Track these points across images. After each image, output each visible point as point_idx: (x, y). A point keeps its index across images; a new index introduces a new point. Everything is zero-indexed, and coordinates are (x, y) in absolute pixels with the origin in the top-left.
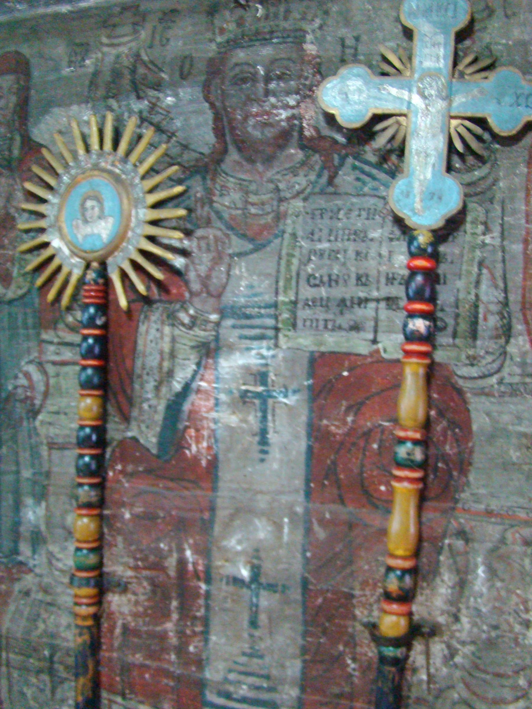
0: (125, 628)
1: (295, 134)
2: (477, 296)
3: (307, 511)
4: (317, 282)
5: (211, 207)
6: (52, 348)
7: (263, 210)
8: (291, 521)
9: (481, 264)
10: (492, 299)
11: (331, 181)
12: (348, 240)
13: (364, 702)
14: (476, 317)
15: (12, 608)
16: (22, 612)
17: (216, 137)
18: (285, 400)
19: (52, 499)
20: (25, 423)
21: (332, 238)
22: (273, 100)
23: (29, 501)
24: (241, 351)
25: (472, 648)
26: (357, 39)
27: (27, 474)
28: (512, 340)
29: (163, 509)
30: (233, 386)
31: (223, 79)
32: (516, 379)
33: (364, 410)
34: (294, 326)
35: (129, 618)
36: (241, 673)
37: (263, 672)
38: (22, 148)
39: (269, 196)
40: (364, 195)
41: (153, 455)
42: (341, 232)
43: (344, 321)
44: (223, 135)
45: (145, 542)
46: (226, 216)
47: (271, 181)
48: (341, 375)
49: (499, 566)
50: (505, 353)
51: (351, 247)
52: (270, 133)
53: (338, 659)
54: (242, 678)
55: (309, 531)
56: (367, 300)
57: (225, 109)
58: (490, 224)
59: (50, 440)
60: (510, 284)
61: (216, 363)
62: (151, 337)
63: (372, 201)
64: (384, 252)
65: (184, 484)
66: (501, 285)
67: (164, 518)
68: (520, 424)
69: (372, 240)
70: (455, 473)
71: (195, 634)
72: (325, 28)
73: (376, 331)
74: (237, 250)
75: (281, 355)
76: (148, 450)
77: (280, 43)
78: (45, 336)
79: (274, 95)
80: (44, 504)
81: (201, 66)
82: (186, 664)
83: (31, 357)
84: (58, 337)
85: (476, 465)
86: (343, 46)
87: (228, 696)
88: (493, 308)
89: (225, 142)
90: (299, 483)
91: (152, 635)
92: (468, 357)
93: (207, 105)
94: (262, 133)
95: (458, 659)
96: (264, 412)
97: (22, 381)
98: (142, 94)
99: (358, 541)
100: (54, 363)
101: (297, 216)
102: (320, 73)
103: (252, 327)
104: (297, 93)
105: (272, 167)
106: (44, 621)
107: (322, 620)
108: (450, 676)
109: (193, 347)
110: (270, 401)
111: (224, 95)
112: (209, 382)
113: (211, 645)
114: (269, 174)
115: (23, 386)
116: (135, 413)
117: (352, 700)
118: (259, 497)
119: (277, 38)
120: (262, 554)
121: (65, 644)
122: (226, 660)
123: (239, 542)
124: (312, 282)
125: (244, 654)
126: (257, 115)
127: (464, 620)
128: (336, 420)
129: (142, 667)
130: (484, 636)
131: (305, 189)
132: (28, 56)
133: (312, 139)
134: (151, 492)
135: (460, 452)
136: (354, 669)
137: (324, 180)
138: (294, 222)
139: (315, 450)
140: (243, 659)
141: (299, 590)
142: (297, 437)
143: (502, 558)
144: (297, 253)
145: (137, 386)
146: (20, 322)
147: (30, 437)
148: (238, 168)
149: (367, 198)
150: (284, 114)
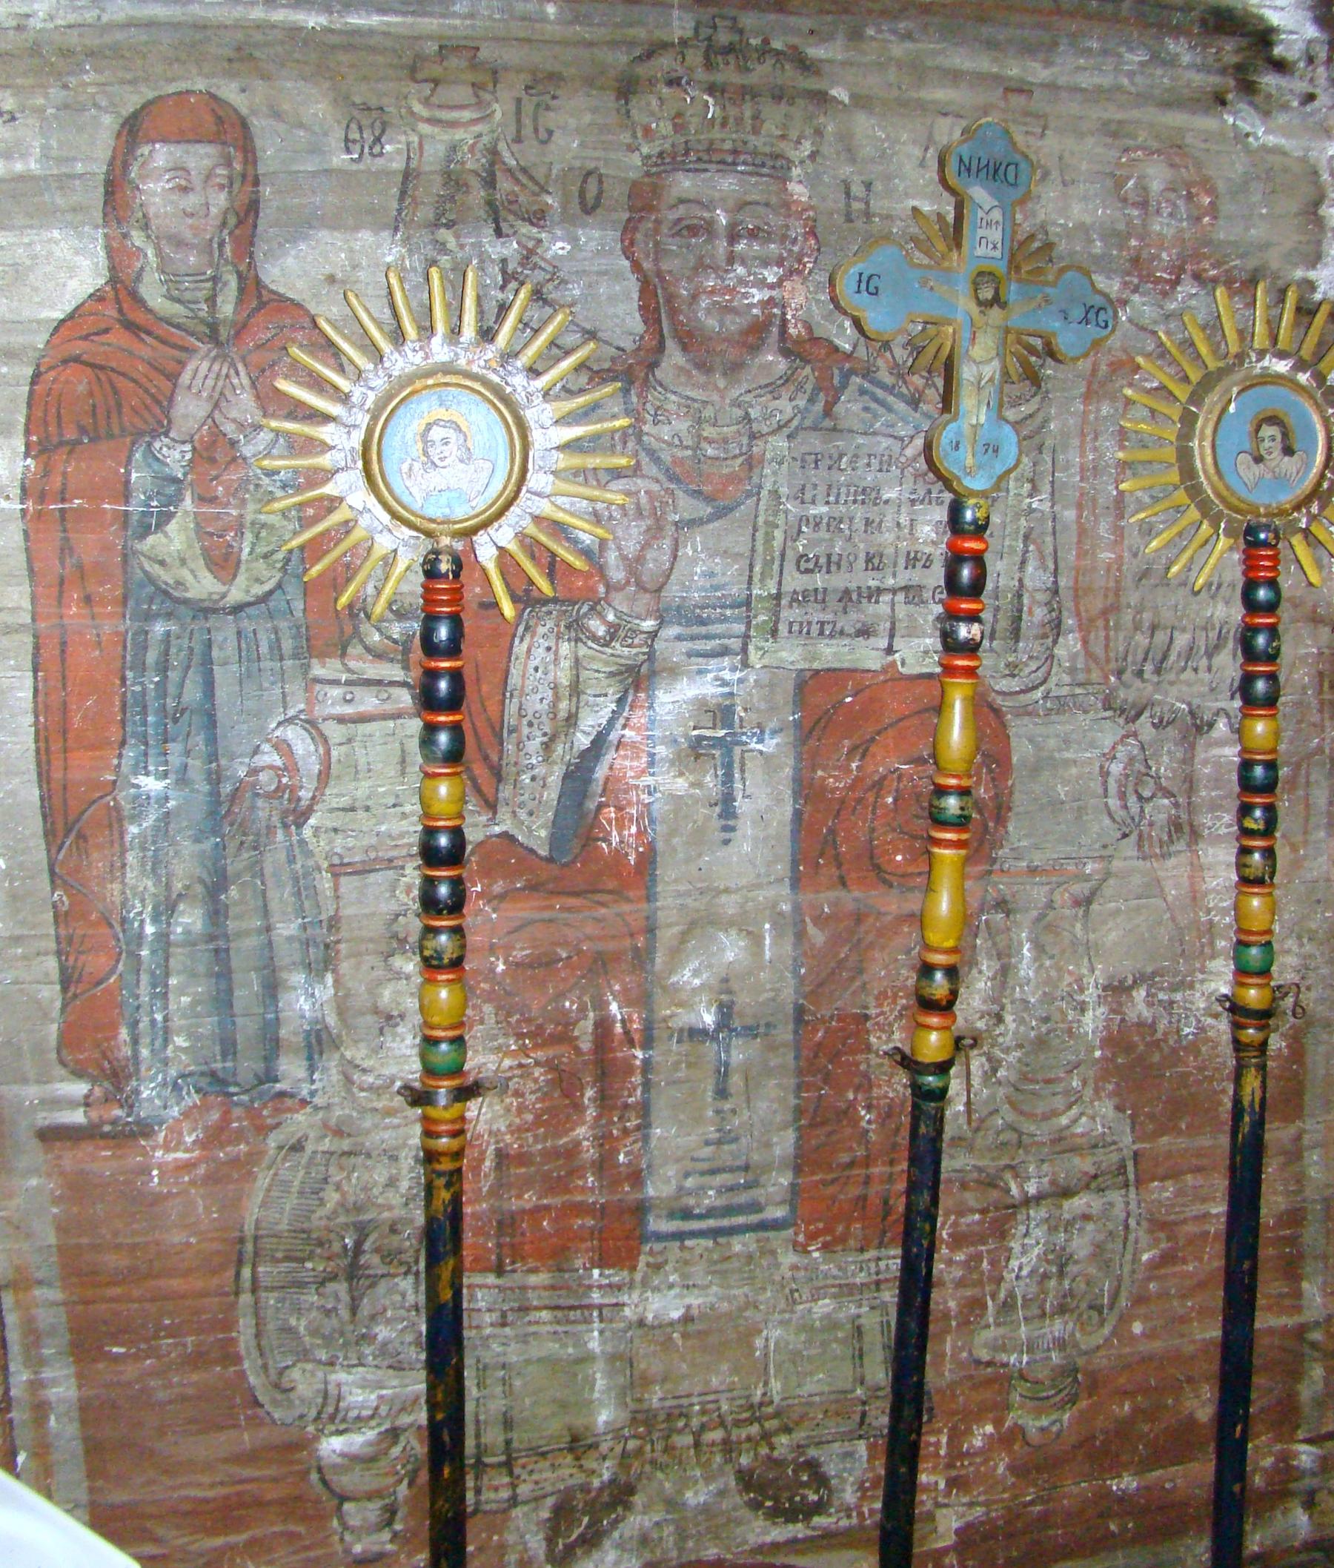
0: (501, 1156)
1: (775, 330)
2: (1020, 580)
3: (797, 908)
4: (811, 566)
5: (639, 441)
6: (336, 692)
7: (726, 451)
8: (775, 925)
9: (1026, 537)
10: (1038, 584)
11: (828, 412)
12: (855, 502)
13: (884, 1164)
14: (1020, 611)
15: (263, 1180)
16: (286, 1184)
17: (645, 322)
18: (760, 747)
19: (345, 967)
20: (280, 836)
21: (832, 499)
22: (740, 270)
23: (298, 978)
24: (688, 674)
25: (1018, 1054)
26: (868, 186)
27: (286, 929)
28: (1061, 640)
29: (565, 944)
30: (679, 731)
31: (658, 222)
32: (1065, 691)
33: (873, 749)
34: (774, 633)
35: (508, 1138)
36: (703, 1173)
37: (738, 1163)
38: (240, 301)
39: (734, 428)
40: (875, 433)
41: (541, 858)
42: (843, 490)
43: (850, 621)
44: (659, 321)
45: (535, 1005)
46: (666, 457)
47: (736, 403)
48: (841, 702)
49: (1047, 939)
50: (1052, 656)
51: (859, 513)
52: (734, 324)
53: (848, 1113)
54: (707, 1179)
55: (800, 935)
56: (879, 591)
57: (659, 274)
58: (1038, 483)
59: (336, 861)
60: (1061, 564)
61: (651, 698)
62: (532, 664)
63: (885, 442)
64: (904, 520)
65: (598, 897)
66: (1051, 566)
67: (569, 958)
68: (1067, 750)
69: (887, 502)
70: (991, 824)
71: (626, 1132)
72: (819, 160)
73: (892, 636)
74: (687, 516)
75: (752, 679)
76: (532, 851)
77: (750, 174)
78: (318, 670)
79: (743, 263)
80: (329, 978)
81: (616, 193)
82: (615, 1183)
83: (291, 713)
84: (349, 670)
85: (1016, 810)
86: (848, 194)
87: (687, 1214)
88: (1041, 597)
89: (662, 336)
90: (782, 868)
91: (554, 1154)
92: (1008, 665)
93: (627, 263)
94: (722, 324)
95: (1001, 1073)
96: (728, 767)
97: (270, 757)
98: (504, 226)
99: (870, 938)
100: (341, 720)
101: (780, 463)
102: (813, 233)
103: (708, 637)
104: (780, 264)
105: (739, 381)
106: (338, 1187)
107: (823, 1060)
108: (993, 1097)
109: (612, 675)
110: (737, 750)
111: (659, 252)
112: (638, 730)
113: (653, 1143)
114: (735, 393)
115: (271, 767)
116: (506, 792)
117: (867, 1166)
118: (724, 898)
119: (745, 163)
120: (735, 985)
121: (386, 1214)
122: (678, 1160)
123: (696, 973)
124: (803, 565)
125: (707, 1143)
126: (713, 292)
127: (1009, 1018)
128: (836, 768)
129: (538, 1211)
130: (1033, 1034)
131: (790, 421)
132: (244, 111)
133: (798, 341)
134: (543, 921)
135: (997, 795)
136: (869, 1122)
137: (819, 407)
138: (775, 473)
139: (806, 816)
140: (707, 1151)
141: (791, 1027)
142: (779, 801)
143: (1049, 927)
144: (780, 521)
145: (510, 747)
146: (264, 649)
147: (291, 860)
148: (683, 379)
149: (879, 438)
150: (757, 295)
